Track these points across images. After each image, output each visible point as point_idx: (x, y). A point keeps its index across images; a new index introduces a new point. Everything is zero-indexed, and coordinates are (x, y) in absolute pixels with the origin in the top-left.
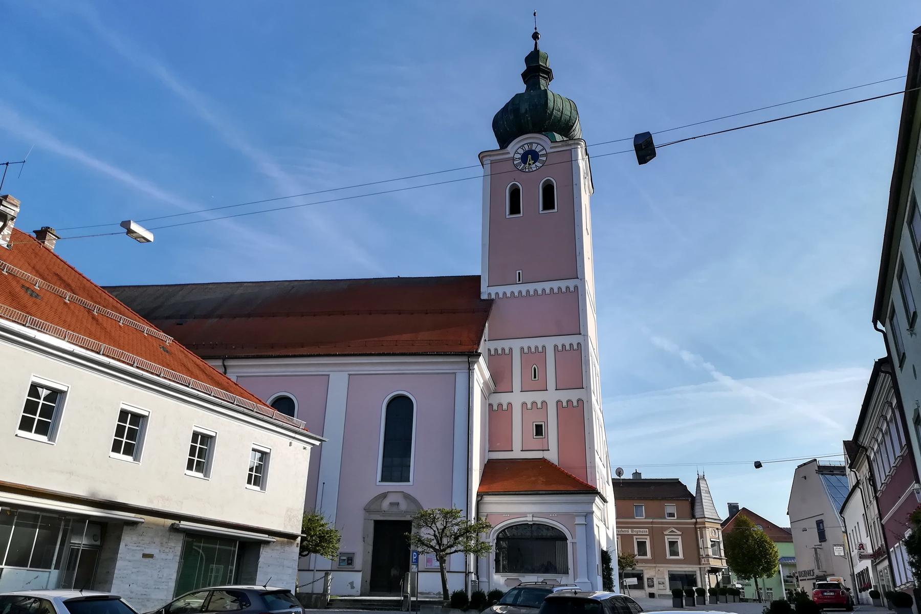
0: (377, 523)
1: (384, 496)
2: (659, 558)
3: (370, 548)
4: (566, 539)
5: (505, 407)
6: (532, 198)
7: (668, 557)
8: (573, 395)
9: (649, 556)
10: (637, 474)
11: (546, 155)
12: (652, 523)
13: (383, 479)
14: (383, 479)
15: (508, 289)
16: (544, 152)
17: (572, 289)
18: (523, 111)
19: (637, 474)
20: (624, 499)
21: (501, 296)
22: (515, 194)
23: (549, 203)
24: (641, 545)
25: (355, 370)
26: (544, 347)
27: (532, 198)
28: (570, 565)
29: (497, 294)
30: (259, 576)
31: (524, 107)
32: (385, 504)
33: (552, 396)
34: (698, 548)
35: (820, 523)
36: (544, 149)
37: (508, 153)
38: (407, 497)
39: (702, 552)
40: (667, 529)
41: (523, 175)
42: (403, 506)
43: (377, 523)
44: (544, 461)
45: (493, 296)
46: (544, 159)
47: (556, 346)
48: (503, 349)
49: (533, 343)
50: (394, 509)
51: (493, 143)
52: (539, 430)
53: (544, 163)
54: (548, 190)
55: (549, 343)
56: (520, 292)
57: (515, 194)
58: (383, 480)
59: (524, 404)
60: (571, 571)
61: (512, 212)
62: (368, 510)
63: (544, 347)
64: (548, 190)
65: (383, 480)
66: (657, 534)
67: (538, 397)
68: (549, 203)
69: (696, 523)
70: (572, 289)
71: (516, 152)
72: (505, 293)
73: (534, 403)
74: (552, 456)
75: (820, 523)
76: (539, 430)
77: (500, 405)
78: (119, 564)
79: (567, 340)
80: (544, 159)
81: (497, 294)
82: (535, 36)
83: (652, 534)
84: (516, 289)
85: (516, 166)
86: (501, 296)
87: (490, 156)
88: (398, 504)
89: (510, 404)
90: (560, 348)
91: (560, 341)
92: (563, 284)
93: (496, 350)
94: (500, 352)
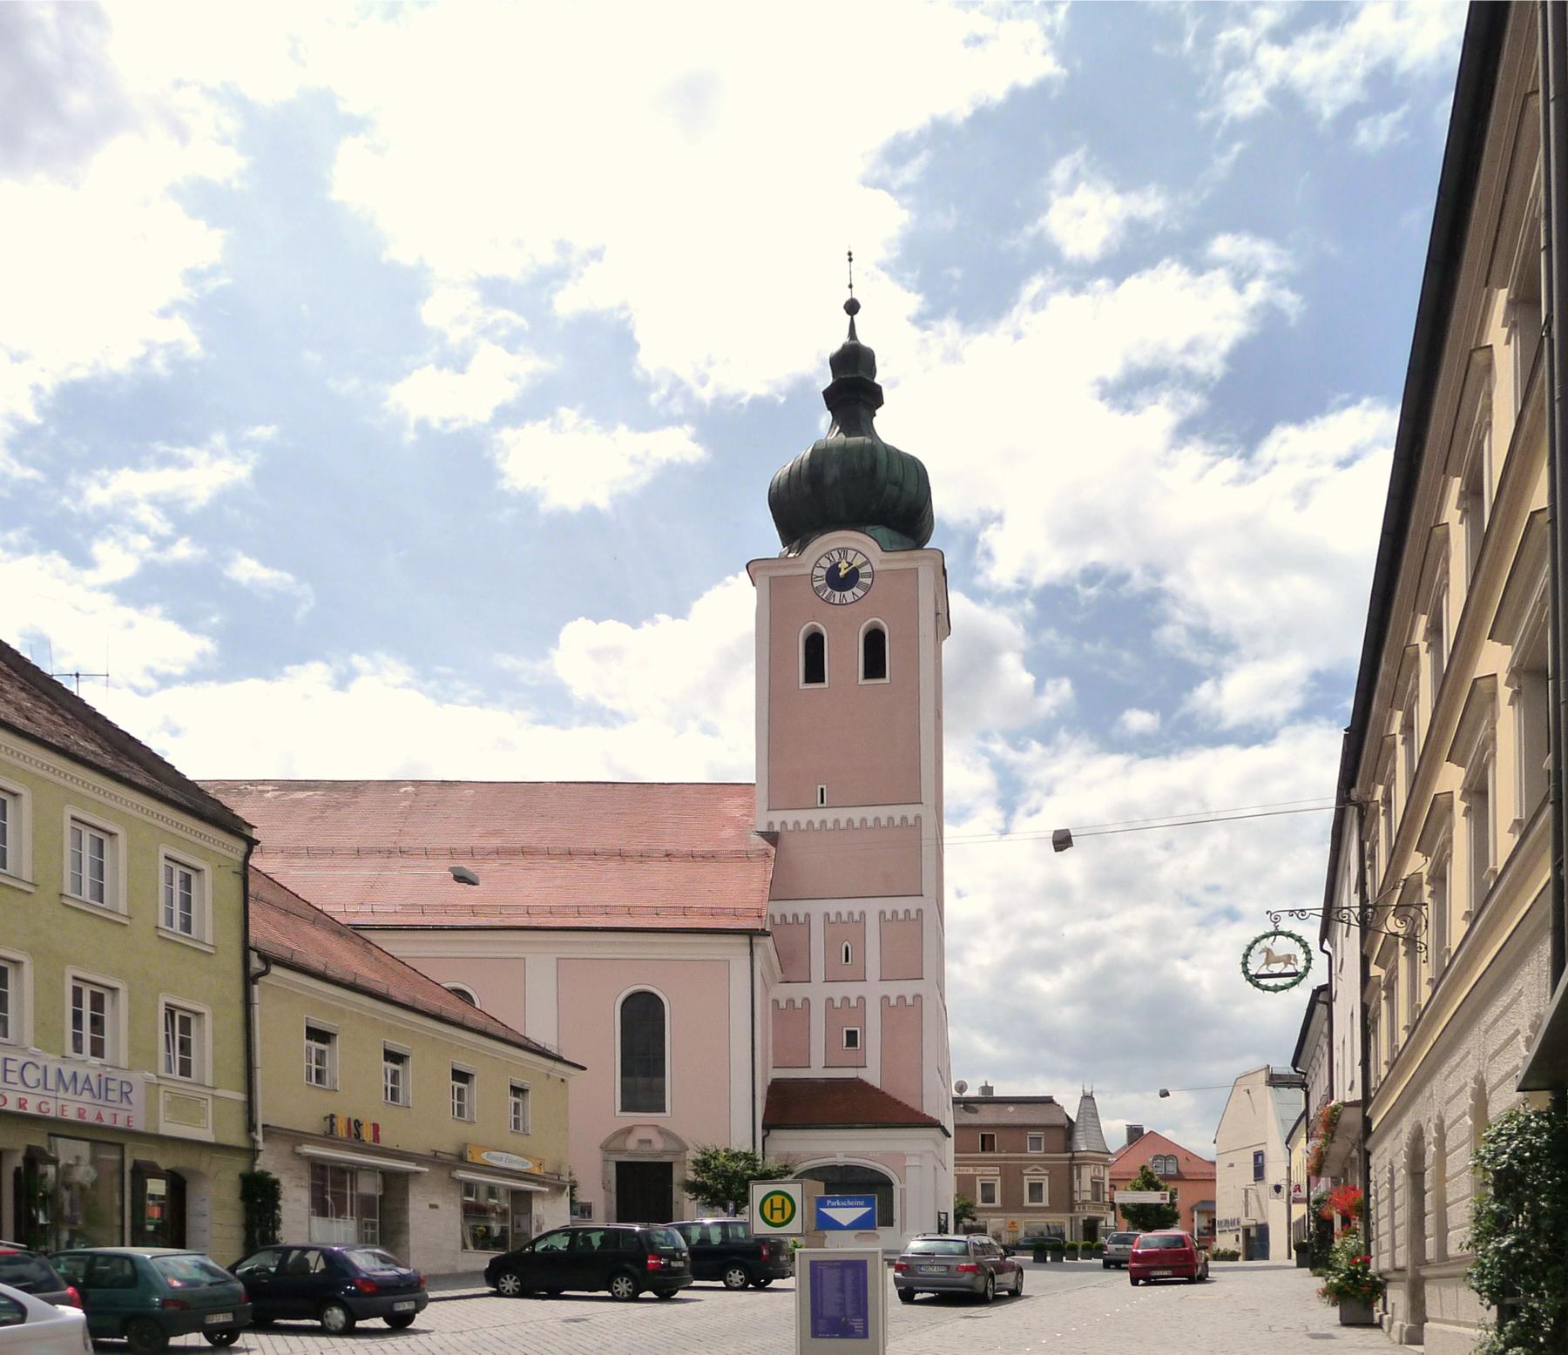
1: (629, 1131)
2: (1012, 1204)
3: (614, 1197)
6: (845, 656)
7: (1027, 1203)
8: (908, 989)
9: (998, 1203)
10: (987, 1089)
11: (872, 575)
13: (625, 1108)
14: (625, 1108)
15: (803, 816)
16: (867, 569)
17: (911, 821)
18: (829, 480)
19: (987, 1089)
20: (899, 1103)
21: (790, 827)
22: (815, 643)
23: (875, 665)
25: (567, 952)
27: (845, 656)
29: (784, 823)
30: (686, 1214)
31: (832, 473)
32: (632, 1143)
35: (1258, 1156)
36: (868, 562)
37: (803, 565)
38: (663, 1132)
40: (1026, 1167)
41: (830, 610)
42: (659, 1144)
43: (619, 1165)
44: (859, 1084)
45: (777, 828)
46: (869, 581)
47: (882, 913)
49: (844, 906)
50: (645, 1148)
51: (770, 542)
52: (852, 1038)
53: (867, 589)
54: (875, 640)
55: (872, 907)
56: (823, 822)
57: (815, 643)
60: (897, 1223)
61: (808, 680)
64: (875, 640)
66: (1012, 1176)
68: (875, 665)
69: (1073, 1158)
70: (911, 821)
71: (817, 565)
75: (1258, 1156)
79: (901, 905)
80: (869, 581)
81: (784, 823)
82: (852, 307)
83: (1004, 1174)
84: (816, 816)
85: (816, 591)
86: (790, 827)
87: (769, 568)
88: (650, 1141)
90: (888, 916)
91: (889, 905)
92: (897, 812)
94: (790, 919)
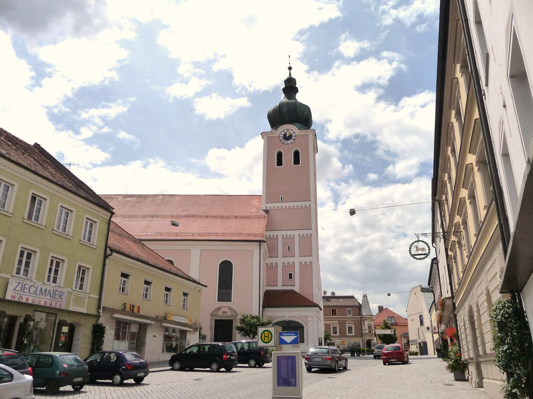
0: (216, 321)
1: (219, 308)
2: (343, 335)
4: (303, 327)
5: (274, 265)
6: (288, 158)
7: (348, 334)
9: (338, 334)
11: (296, 136)
12: (340, 318)
13: (219, 300)
14: (219, 300)
15: (276, 205)
16: (294, 134)
17: (308, 206)
18: (284, 111)
22: (280, 155)
23: (297, 161)
24: (335, 328)
26: (294, 235)
27: (288, 158)
28: (305, 339)
31: (285, 109)
32: (220, 313)
33: (280, 260)
34: (362, 330)
35: (421, 316)
36: (294, 133)
38: (230, 309)
39: (363, 332)
41: (284, 146)
42: (229, 313)
43: (216, 321)
44: (293, 292)
45: (268, 209)
48: (273, 236)
49: (288, 233)
50: (225, 314)
51: (268, 127)
52: (291, 275)
54: (297, 154)
55: (296, 233)
57: (280, 155)
58: (218, 301)
59: (301, 263)
60: (305, 342)
62: (212, 315)
63: (294, 235)
64: (297, 154)
65: (218, 301)
66: (342, 324)
67: (286, 260)
68: (297, 161)
69: (361, 318)
70: (308, 206)
72: (274, 207)
73: (306, 262)
74: (297, 289)
75: (421, 316)
76: (291, 275)
77: (272, 264)
78: (147, 339)
79: (305, 232)
81: (270, 207)
85: (280, 140)
89: (276, 263)
91: (302, 232)
92: (303, 204)
93: (270, 236)
94: (272, 237)
